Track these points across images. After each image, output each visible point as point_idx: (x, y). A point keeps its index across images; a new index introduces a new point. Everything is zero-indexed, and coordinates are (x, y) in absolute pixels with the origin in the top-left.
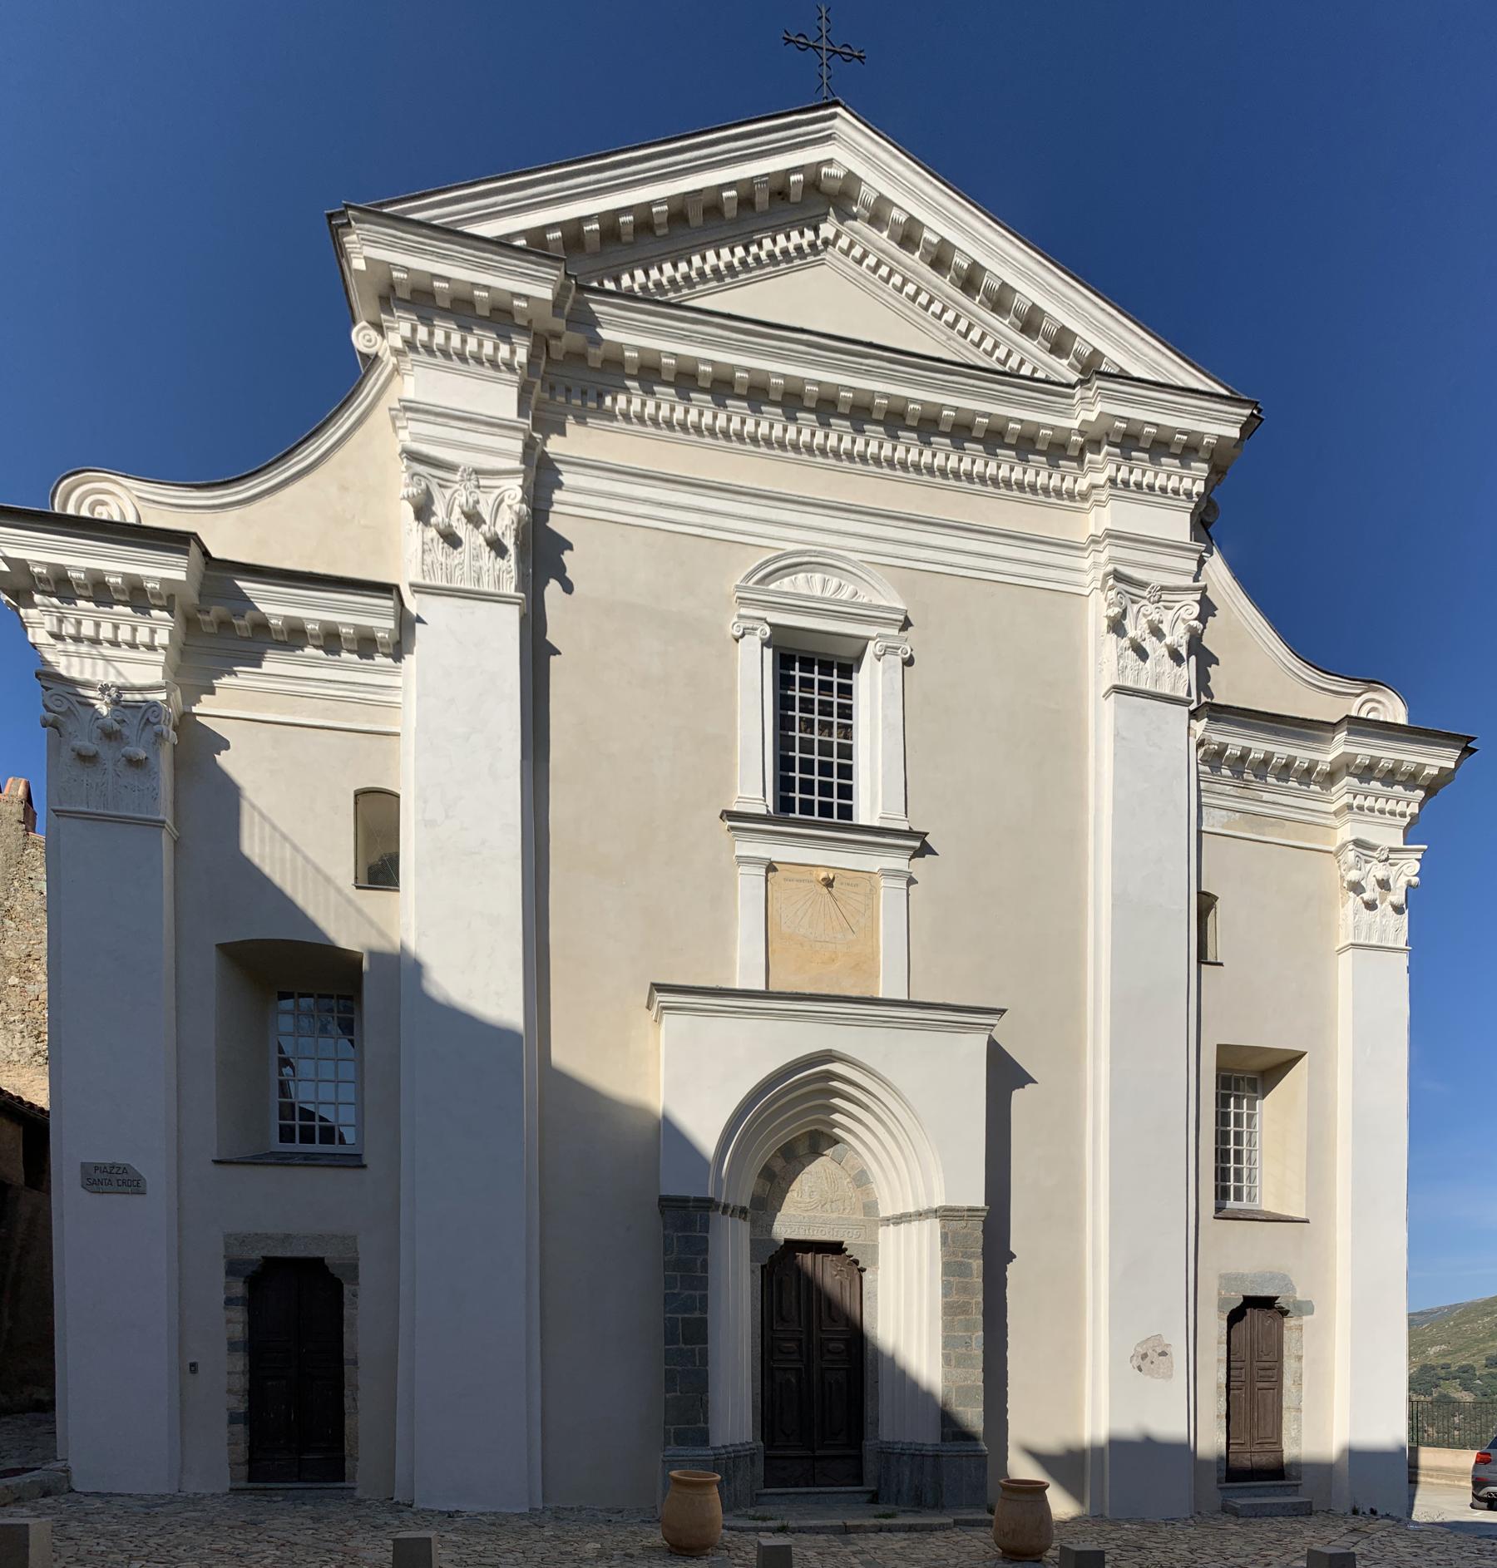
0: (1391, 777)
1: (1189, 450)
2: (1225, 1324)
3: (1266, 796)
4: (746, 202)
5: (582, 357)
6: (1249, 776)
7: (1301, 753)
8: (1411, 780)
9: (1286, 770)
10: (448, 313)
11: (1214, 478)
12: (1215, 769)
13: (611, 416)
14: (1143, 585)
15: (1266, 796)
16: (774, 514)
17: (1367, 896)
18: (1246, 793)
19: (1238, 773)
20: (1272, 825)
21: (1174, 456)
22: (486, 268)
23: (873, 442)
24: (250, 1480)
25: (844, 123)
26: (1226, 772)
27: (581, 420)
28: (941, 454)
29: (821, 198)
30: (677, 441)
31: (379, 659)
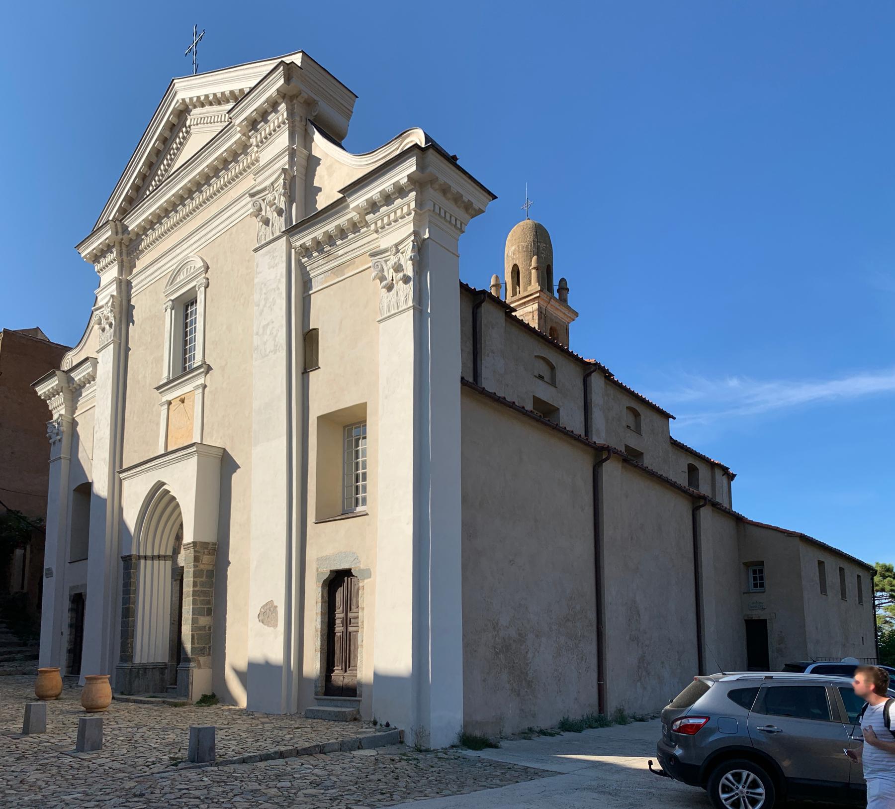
0: (388, 199)
1: (274, 105)
2: (691, 512)
3: (340, 253)
4: (167, 134)
5: (131, 240)
6: (327, 248)
7: (342, 220)
8: (400, 191)
9: (342, 233)
10: (101, 257)
11: (290, 107)
12: (310, 256)
13: (142, 251)
14: (264, 189)
15: (340, 253)
16: (185, 246)
17: (401, 275)
18: (331, 257)
19: (321, 251)
20: (348, 266)
21: (271, 112)
22: (99, 238)
23: (225, 176)
24: (325, 695)
25: (179, 84)
26: (315, 254)
27: (138, 259)
28: (216, 184)
29: (183, 112)
30: (180, 228)
31: (351, 236)
